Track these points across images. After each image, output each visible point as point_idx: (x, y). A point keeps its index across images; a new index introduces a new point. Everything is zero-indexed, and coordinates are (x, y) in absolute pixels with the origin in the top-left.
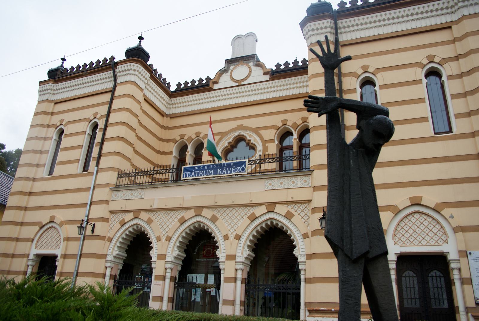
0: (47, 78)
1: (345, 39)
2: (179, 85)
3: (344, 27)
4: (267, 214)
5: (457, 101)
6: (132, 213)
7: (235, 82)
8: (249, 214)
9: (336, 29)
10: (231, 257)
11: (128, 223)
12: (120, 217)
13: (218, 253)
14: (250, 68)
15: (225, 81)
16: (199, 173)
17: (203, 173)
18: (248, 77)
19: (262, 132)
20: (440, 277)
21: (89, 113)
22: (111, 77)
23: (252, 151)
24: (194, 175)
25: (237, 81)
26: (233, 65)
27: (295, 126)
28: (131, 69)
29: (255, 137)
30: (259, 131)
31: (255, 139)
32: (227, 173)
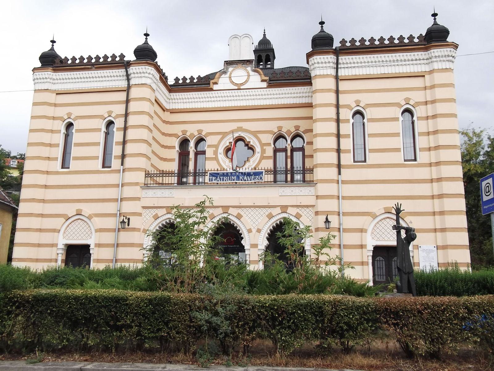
0: (39, 65)
1: (343, 74)
2: (177, 79)
3: (343, 63)
4: (281, 214)
5: (421, 137)
6: (165, 209)
7: (234, 85)
8: (267, 213)
9: (337, 63)
10: (254, 246)
11: (161, 218)
12: (154, 212)
13: (243, 242)
14: (248, 73)
15: (223, 82)
16: (223, 179)
17: (227, 179)
18: (246, 82)
19: (260, 136)
20: (382, 261)
21: (103, 110)
22: (123, 76)
23: (251, 151)
24: (219, 180)
25: (236, 84)
26: (231, 67)
27: (289, 132)
28: (146, 73)
29: (253, 139)
30: (258, 135)
31: (253, 141)
32: (248, 180)
